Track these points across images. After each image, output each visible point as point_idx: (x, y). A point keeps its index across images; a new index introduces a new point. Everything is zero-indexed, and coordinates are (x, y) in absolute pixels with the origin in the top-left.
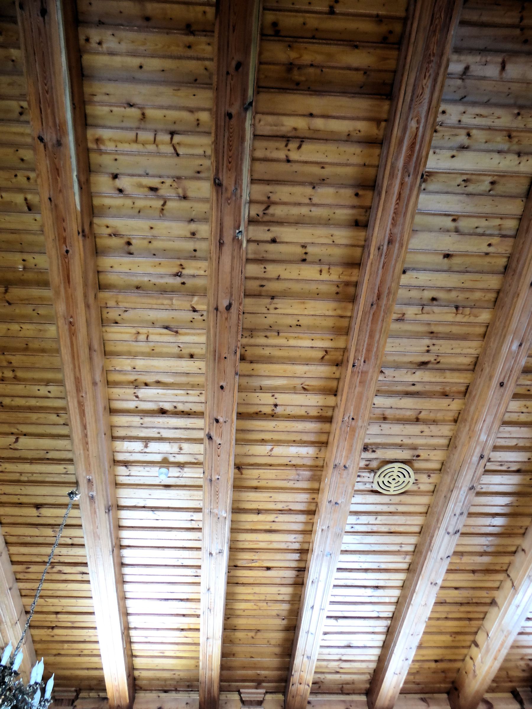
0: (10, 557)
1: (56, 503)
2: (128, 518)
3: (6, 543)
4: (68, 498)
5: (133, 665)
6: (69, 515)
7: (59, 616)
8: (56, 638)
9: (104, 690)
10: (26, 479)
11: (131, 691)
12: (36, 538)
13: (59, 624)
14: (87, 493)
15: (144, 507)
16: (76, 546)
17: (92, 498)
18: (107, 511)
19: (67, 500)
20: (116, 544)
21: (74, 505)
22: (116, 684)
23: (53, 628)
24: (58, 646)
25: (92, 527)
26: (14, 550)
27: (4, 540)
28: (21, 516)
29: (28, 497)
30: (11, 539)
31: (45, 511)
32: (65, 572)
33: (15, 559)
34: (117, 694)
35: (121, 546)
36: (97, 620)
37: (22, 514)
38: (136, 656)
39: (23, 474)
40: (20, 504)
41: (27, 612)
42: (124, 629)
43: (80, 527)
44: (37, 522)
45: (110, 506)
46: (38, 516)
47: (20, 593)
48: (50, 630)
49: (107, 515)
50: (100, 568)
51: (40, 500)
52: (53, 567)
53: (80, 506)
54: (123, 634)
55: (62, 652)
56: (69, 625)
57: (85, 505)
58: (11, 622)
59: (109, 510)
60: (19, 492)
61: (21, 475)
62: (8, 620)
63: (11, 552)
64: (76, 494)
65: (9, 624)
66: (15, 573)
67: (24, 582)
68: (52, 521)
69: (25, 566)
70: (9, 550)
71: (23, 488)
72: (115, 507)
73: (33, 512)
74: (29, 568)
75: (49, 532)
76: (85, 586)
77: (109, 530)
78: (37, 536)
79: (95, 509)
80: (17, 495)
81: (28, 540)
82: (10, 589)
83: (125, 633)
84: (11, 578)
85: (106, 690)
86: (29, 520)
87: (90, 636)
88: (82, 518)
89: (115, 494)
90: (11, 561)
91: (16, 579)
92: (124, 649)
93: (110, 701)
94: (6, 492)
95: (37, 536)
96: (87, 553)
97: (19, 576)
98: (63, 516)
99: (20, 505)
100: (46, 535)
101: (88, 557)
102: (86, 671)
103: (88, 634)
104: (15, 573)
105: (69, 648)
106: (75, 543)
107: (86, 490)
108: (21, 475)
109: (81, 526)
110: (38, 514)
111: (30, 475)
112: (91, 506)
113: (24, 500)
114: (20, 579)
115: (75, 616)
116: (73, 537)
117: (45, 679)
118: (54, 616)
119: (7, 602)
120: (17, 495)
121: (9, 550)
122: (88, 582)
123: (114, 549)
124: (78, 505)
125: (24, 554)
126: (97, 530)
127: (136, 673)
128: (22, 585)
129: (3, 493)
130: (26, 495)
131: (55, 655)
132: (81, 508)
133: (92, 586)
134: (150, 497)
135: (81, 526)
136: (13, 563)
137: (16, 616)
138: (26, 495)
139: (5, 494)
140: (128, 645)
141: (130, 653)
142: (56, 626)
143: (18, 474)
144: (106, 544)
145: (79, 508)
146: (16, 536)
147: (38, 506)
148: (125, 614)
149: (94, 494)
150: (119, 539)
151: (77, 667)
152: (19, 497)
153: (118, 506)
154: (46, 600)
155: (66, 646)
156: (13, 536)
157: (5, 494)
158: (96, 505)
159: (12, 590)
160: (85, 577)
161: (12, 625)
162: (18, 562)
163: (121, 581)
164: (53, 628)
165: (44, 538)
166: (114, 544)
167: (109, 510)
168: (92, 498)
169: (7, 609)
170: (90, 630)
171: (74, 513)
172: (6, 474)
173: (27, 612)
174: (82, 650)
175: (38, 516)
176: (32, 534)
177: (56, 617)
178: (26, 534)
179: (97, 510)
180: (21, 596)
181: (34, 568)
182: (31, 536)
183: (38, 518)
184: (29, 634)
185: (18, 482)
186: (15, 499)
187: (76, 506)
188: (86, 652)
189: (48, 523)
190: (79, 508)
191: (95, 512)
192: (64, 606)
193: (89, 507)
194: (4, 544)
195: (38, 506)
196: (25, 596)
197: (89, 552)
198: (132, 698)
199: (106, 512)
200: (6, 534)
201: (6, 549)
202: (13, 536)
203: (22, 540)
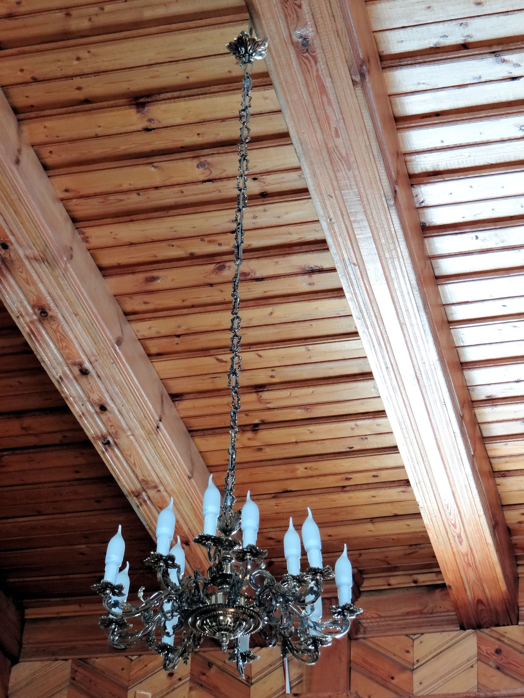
0: (93, 256)
1: (192, 80)
2: (420, 88)
3: (74, 220)
4: (232, 58)
5: (498, 496)
6: (250, 110)
7: (266, 395)
8: (269, 453)
9: (431, 564)
10: (85, 24)
11: (507, 563)
12: (154, 194)
13: (268, 416)
14: (285, 34)
15: (465, 46)
16: (276, 199)
17: (304, 48)
18: (358, 78)
19: (229, 65)
20: (398, 173)
21: (256, 76)
22: (464, 548)
23: (255, 428)
24: (279, 471)
25: (320, 136)
26: (99, 235)
27: (65, 214)
28: (97, 137)
29: (103, 77)
30: (85, 208)
31: (164, 112)
32: (258, 275)
33: (109, 259)
34: (471, 574)
35: (411, 176)
36: (384, 390)
37: (99, 131)
38: (505, 474)
39: (75, 12)
40: (87, 101)
41: (176, 397)
42: (463, 407)
43: (282, 141)
44: (147, 148)
45: (363, 62)
46: (147, 130)
47: (145, 348)
48: (250, 435)
49: (359, 91)
50: (367, 248)
51: (141, 81)
52: (221, 268)
53: (274, 77)
54: (461, 419)
55: (292, 486)
56: (299, 414)
57: (287, 69)
58: (143, 427)
59: (362, 76)
60: (75, 67)
61: (68, 15)
62: (134, 423)
63: (94, 242)
64: (255, 44)
65: (140, 432)
66: (118, 297)
67: (150, 319)
68: (189, 138)
69: (141, 276)
70: (86, 240)
71: (83, 53)
72: (374, 63)
73: (130, 118)
74: (154, 279)
75: (188, 169)
76: (327, 306)
77: (372, 135)
78: (157, 188)
79: (318, 77)
80: (71, 77)
81: (133, 201)
82: (119, 342)
83: (467, 417)
84: (112, 310)
85: (437, 565)
86: (124, 146)
87: (364, 437)
88: (286, 112)
89: (367, 20)
90: (101, 269)
91: (126, 314)
92: (472, 458)
93: (454, 592)
94: (39, 73)
95: (157, 188)
96: (321, 212)
97: (133, 305)
98: (237, 113)
99: (87, 104)
100: (182, 180)
101: (324, 224)
102: (370, 526)
103: (357, 432)
104: (118, 297)
105: (310, 473)
106: (270, 188)
107: (282, 24)
108: (68, 15)
109: (285, 135)
110: (145, 124)
111: (94, 10)
112: (306, 71)
113: (95, 87)
114: (135, 313)
115: (310, 390)
116: (262, 173)
117: (330, 552)
118: (253, 397)
119: (119, 378)
120: (71, 77)
121: (86, 240)
122: (337, 292)
123: (397, 188)
124: (266, 75)
125: (131, 244)
126: (339, 141)
127: (513, 517)
128: (144, 328)
129: (28, 77)
130: (97, 73)
131: (276, 496)
132: (276, 82)
133: (350, 303)
134: (479, 11)
135: (285, 135)
136: (105, 271)
137: (151, 409)
138: (97, 73)
139: (35, 80)
140: (479, 446)
141: (487, 468)
142: (263, 423)
143: (60, 15)
144: (376, 177)
145: (270, 84)
146: (95, 195)
147: (140, 100)
148: (456, 366)
149: (309, 31)
150: (403, 156)
151: (340, 518)
152: (78, 81)
153: (382, 58)
154: (219, 357)
155: (300, 469)
156: (88, 197)
157: (35, 80)
158: (321, 65)
159: (123, 344)
160: (322, 282)
161: (149, 433)
162: (120, 266)
163: (431, 279)
164: (255, 428)
165: (177, 189)
166: (393, 174)
167: (362, 76)
168: (304, 48)
169: (124, 395)
170: (359, 423)
171: (260, 99)
172: (30, 20)
173: (176, 397)
174: (347, 475)
175: (147, 130)
176: (140, 184)
177: (260, 400)
178: (126, 186)
179: (327, 82)
180: (149, 355)
181: (167, 278)
182: (138, 191)
183: (148, 136)
184: (195, 450)
185: (64, 37)
186: (66, 91)
187: (263, 80)
188: (358, 479)
189: (180, 144)
190: (270, 84)
191: (323, 90)
192: (273, 368)
193: (300, 78)
194: (70, 223)
195: (140, 100)
196: (159, 354)
197: (325, 207)
198: (513, 581)
199: (354, 82)
200: (67, 195)
201: (79, 237)
202: (88, 197)
203: (115, 204)
